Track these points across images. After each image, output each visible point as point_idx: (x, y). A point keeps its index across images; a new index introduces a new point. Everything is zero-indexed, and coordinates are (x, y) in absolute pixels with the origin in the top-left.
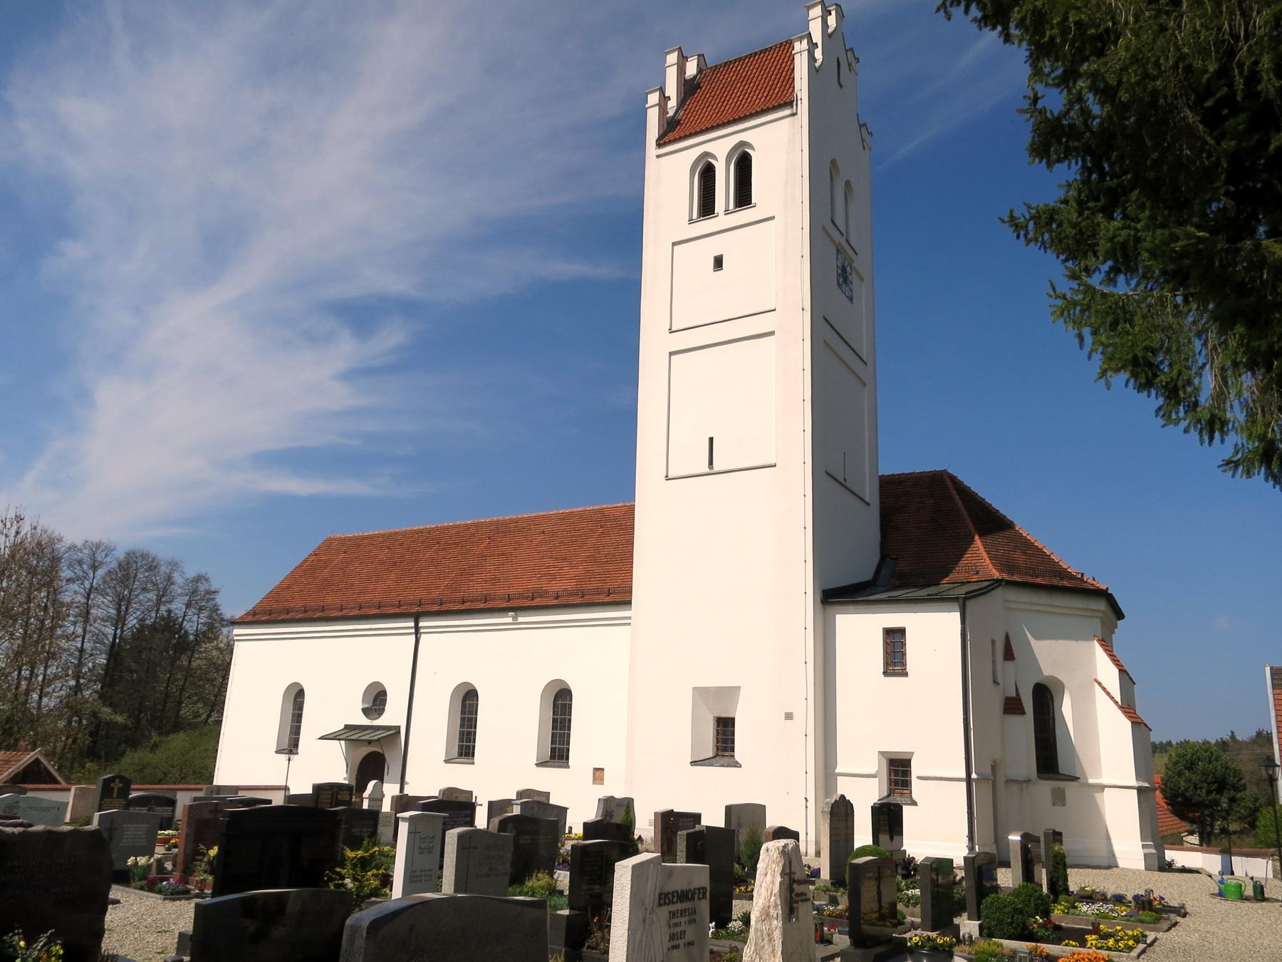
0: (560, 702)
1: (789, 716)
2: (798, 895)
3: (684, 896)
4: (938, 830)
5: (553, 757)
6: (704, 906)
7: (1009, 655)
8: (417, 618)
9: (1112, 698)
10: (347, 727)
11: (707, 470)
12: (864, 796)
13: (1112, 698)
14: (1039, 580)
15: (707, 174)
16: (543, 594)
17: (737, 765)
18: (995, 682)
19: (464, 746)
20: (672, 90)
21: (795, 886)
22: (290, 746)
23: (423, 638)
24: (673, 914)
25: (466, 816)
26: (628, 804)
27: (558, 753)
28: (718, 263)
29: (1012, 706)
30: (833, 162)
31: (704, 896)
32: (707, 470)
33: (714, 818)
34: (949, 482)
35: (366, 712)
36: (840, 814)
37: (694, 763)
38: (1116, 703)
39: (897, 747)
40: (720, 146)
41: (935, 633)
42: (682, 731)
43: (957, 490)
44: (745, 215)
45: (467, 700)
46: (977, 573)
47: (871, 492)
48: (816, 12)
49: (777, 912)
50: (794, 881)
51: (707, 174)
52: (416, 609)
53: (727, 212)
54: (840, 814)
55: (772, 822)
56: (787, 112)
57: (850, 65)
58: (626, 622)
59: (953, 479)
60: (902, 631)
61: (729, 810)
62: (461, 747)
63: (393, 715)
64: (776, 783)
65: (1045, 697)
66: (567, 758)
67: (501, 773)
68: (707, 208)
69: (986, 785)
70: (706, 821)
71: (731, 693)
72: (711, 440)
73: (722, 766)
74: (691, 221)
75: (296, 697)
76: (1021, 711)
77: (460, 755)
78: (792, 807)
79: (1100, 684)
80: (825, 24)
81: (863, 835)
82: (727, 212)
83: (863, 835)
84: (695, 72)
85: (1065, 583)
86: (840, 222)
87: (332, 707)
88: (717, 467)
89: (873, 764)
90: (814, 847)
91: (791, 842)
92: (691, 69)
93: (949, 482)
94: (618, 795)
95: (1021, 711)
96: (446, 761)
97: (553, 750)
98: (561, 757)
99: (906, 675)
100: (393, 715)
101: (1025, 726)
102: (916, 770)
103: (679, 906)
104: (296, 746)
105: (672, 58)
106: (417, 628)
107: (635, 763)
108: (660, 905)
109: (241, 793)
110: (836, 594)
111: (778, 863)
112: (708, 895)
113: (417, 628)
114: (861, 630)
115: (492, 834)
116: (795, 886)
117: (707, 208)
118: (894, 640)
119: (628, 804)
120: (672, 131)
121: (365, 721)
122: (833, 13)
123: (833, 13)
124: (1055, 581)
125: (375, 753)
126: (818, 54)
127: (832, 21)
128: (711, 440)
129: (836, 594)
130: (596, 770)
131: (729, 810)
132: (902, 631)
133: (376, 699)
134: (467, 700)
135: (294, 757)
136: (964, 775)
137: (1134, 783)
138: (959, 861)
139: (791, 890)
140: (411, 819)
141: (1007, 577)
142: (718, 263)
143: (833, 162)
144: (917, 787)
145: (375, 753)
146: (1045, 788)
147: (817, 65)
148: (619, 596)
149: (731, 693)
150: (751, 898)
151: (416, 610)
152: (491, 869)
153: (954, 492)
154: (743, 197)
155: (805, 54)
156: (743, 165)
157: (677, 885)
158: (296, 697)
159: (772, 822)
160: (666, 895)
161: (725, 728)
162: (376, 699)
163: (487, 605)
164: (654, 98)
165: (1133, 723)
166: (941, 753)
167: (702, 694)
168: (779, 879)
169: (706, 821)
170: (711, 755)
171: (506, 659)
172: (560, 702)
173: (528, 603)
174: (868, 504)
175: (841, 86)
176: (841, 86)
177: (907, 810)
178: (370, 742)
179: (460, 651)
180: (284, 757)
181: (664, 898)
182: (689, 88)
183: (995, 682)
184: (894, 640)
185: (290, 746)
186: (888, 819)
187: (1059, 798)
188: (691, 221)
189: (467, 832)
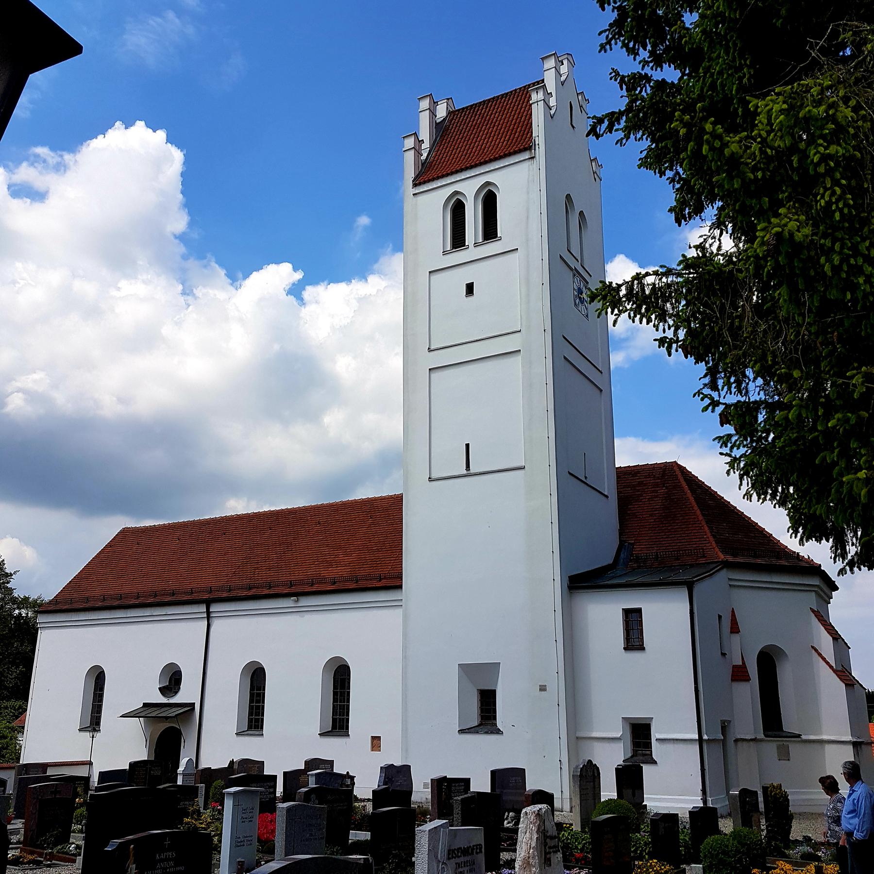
0: (340, 677)
1: (543, 688)
2: (550, 848)
3: (465, 851)
4: (673, 789)
5: (334, 727)
6: (481, 858)
7: (735, 629)
8: (208, 603)
9: (827, 663)
10: (145, 705)
11: (465, 472)
12: (610, 759)
13: (827, 663)
14: (759, 561)
15: (458, 210)
16: (322, 581)
17: (498, 732)
18: (723, 654)
19: (254, 720)
20: (425, 134)
21: (548, 840)
22: (93, 723)
23: (216, 624)
24: (458, 865)
25: (270, 787)
26: (406, 770)
27: (338, 723)
28: (470, 289)
29: (739, 674)
30: (568, 197)
31: (481, 852)
32: (465, 472)
33: (481, 784)
34: (678, 472)
35: (164, 691)
36: (587, 777)
37: (461, 731)
38: (831, 667)
39: (638, 713)
40: (469, 187)
41: (667, 615)
42: (450, 703)
43: (686, 480)
44: (493, 248)
45: (256, 678)
46: (704, 557)
47: (609, 486)
48: (551, 63)
49: (535, 861)
50: (548, 837)
51: (458, 210)
52: (206, 596)
53: (476, 245)
54: (587, 777)
55: (531, 785)
56: (526, 155)
57: (581, 107)
58: (396, 605)
59: (683, 469)
60: (639, 611)
61: (496, 775)
62: (250, 721)
63: (187, 693)
64: (534, 750)
65: (768, 661)
66: (347, 728)
67: (288, 744)
68: (458, 241)
69: (716, 743)
70: (474, 788)
71: (493, 668)
72: (467, 446)
73: (486, 733)
74: (445, 253)
75: (98, 679)
76: (746, 678)
77: (250, 727)
78: (548, 774)
79: (816, 650)
80: (558, 74)
81: (609, 791)
82: (476, 245)
83: (609, 791)
84: (444, 114)
85: (784, 563)
86: (576, 251)
87: (133, 687)
88: (473, 469)
89: (618, 730)
90: (566, 806)
91: (544, 807)
92: (442, 112)
93: (678, 472)
94: (398, 763)
95: (746, 678)
96: (80, 730)
97: (334, 720)
98: (341, 728)
99: (644, 649)
100: (187, 693)
101: (748, 695)
102: (655, 734)
103: (462, 859)
104: (98, 724)
105: (425, 104)
106: (208, 612)
107: (405, 734)
108: (449, 859)
109: (50, 772)
110: (580, 582)
111: (535, 823)
112: (483, 850)
113: (208, 612)
114: (604, 613)
115: (351, 809)
116: (548, 840)
117: (458, 241)
118: (633, 620)
119: (406, 770)
120: (426, 174)
121: (163, 700)
122: (565, 62)
123: (565, 62)
124: (774, 561)
125: (170, 725)
126: (552, 102)
127: (564, 69)
128: (467, 446)
129: (580, 582)
130: (373, 738)
131: (496, 775)
132: (639, 611)
133: (172, 680)
134: (256, 678)
135: (98, 735)
136: (696, 737)
137: (849, 738)
138: (684, 816)
139: (546, 844)
140: (235, 794)
141: (731, 559)
142: (470, 289)
143: (568, 197)
144: (657, 750)
145: (170, 725)
146: (771, 748)
147: (552, 112)
148: (391, 581)
149: (493, 668)
150: (515, 851)
151: (207, 598)
152: (311, 835)
153: (684, 484)
154: (490, 232)
155: (541, 104)
156: (489, 202)
157: (461, 843)
158: (98, 679)
159: (531, 785)
160: (453, 851)
161: (488, 701)
162: (172, 680)
163: (272, 592)
164: (410, 143)
165: (846, 685)
166: (676, 723)
167: (468, 671)
168: (535, 836)
169: (474, 788)
170: (476, 724)
171: (291, 640)
172: (340, 677)
173: (309, 589)
174: (607, 497)
175: (573, 127)
176: (573, 127)
177: (646, 769)
178: (167, 718)
179: (247, 634)
180: (88, 735)
181: (452, 853)
182: (440, 130)
183: (723, 654)
184: (633, 620)
185: (93, 723)
186: (630, 778)
187: (784, 754)
188: (445, 253)
189: (293, 806)
